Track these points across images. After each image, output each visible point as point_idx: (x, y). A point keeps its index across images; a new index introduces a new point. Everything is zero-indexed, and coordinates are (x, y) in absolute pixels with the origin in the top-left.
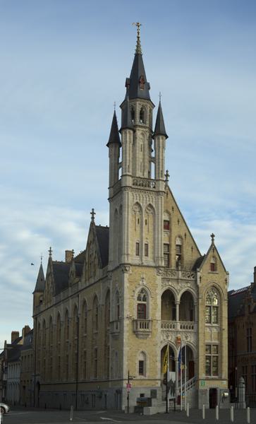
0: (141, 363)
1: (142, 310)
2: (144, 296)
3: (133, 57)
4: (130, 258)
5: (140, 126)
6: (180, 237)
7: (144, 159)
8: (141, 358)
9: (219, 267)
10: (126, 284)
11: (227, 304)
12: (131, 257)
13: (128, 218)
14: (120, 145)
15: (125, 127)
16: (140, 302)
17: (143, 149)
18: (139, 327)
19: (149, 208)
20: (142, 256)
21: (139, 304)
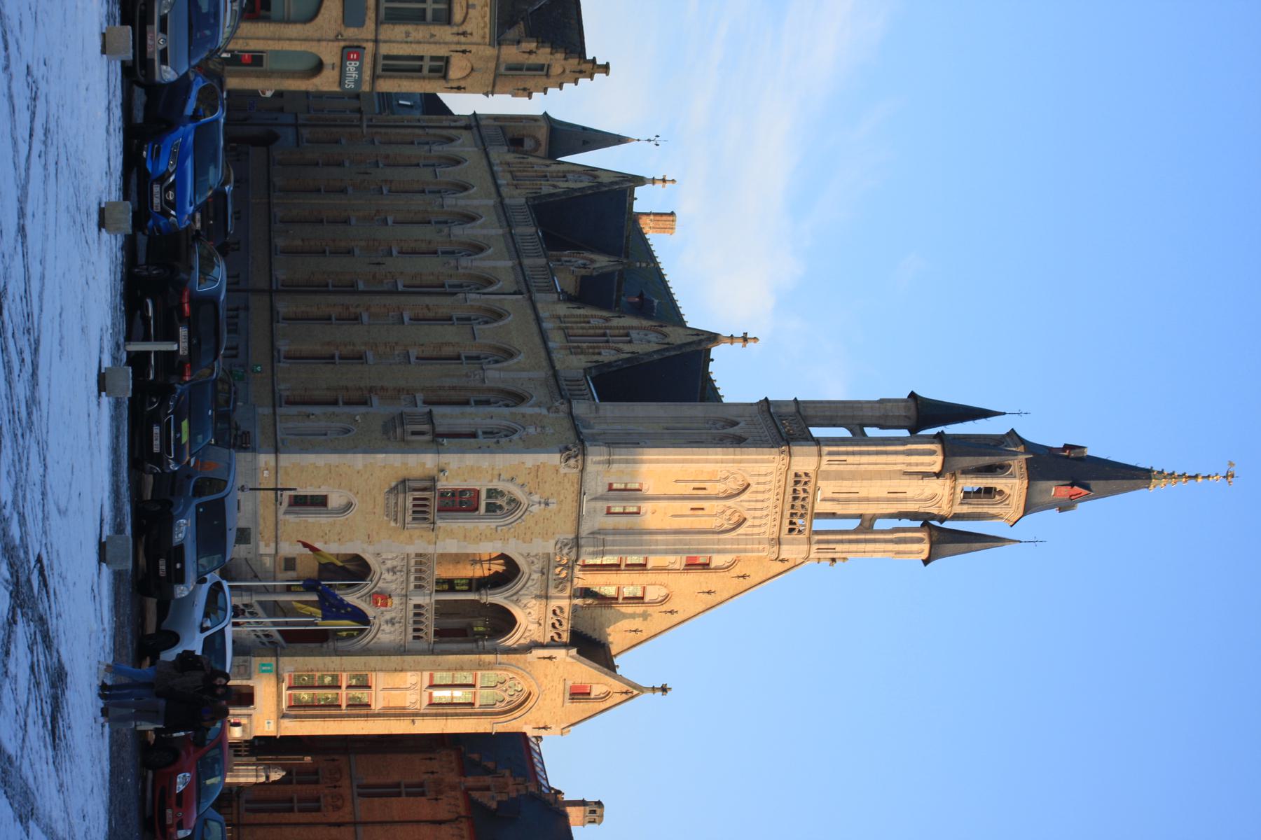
0: (319, 502)
1: (461, 503)
2: (501, 507)
3: (1144, 464)
4: (600, 467)
5: (954, 488)
6: (666, 598)
7: (868, 500)
8: (335, 501)
9: (583, 707)
10: (530, 460)
11: (481, 730)
12: (601, 469)
13: (707, 461)
14: (913, 430)
15: (952, 447)
16: (483, 495)
17: (894, 497)
18: (418, 494)
19: (735, 518)
20: (607, 499)
21: (478, 492)
